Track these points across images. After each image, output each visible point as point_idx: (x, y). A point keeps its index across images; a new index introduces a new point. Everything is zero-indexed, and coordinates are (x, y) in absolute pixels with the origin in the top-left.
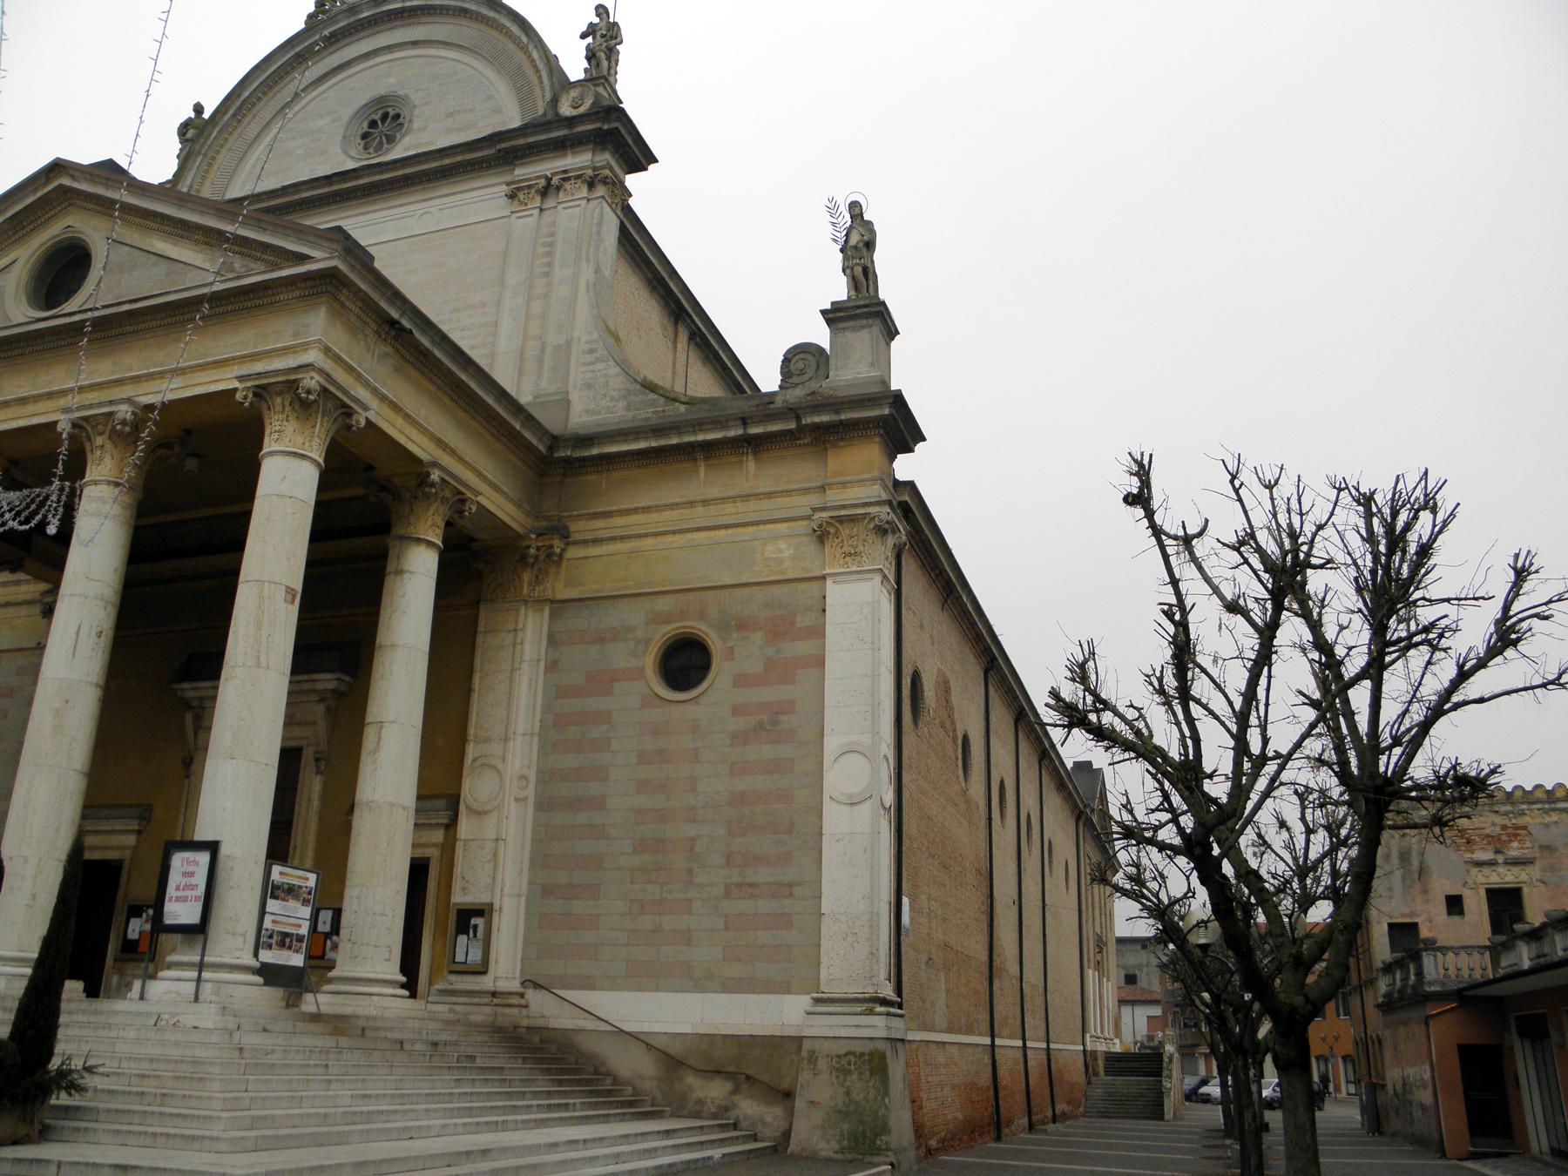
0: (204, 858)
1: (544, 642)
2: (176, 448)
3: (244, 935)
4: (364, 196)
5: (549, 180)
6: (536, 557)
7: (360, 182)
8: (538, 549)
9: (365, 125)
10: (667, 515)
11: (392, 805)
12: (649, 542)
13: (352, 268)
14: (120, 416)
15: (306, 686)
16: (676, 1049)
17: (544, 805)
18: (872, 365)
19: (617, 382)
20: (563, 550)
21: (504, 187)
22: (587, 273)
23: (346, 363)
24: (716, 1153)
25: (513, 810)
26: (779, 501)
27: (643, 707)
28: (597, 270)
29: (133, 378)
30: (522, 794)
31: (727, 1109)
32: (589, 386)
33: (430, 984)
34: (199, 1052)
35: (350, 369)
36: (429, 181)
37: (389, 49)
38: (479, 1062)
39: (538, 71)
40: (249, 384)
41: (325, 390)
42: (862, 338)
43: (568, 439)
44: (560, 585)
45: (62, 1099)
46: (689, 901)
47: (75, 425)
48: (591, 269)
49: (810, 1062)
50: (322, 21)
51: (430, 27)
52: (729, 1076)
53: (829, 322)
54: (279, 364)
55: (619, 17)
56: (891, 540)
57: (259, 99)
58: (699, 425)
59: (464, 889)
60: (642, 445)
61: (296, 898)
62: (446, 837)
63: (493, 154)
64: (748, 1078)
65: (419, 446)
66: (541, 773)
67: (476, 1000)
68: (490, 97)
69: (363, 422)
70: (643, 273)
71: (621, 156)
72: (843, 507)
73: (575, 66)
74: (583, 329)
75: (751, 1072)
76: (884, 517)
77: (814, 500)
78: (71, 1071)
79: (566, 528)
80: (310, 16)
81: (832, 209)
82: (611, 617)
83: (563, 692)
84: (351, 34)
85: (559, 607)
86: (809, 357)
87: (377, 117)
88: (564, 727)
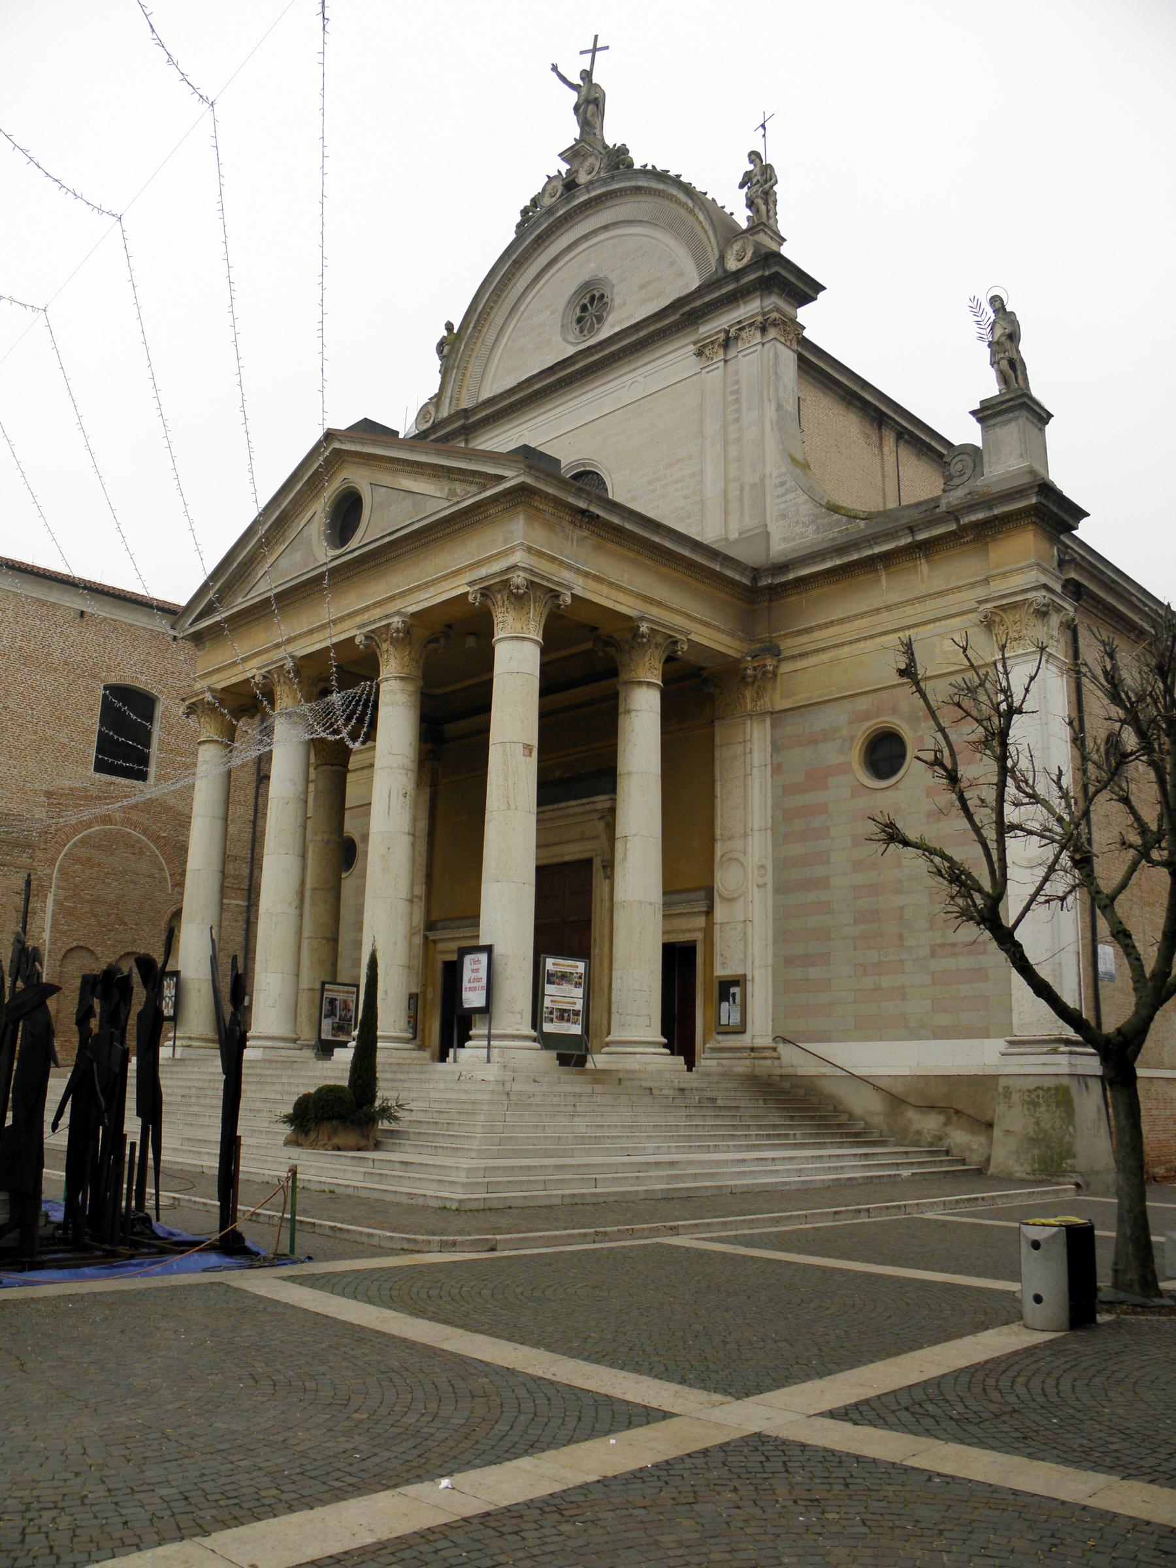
0: (483, 957)
1: (769, 749)
2: (442, 641)
3: (521, 1013)
4: (582, 377)
5: (727, 332)
6: (755, 677)
7: (577, 366)
8: (755, 669)
9: (578, 310)
10: (858, 623)
11: (640, 902)
12: (846, 650)
13: (537, 478)
14: (394, 626)
15: (588, 807)
16: (898, 1089)
17: (781, 888)
18: (1021, 456)
19: (807, 509)
20: (776, 667)
21: (692, 347)
22: (770, 412)
23: (548, 555)
24: (905, 1173)
25: (756, 895)
26: (951, 598)
27: (853, 796)
28: (779, 408)
29: (400, 593)
30: (761, 881)
31: (940, 1139)
32: (783, 516)
33: (704, 1044)
34: (479, 1096)
35: (553, 559)
36: (632, 353)
37: (585, 237)
38: (720, 1103)
39: (706, 232)
40: (476, 588)
41: (532, 582)
42: (1012, 431)
43: (766, 570)
44: (777, 698)
45: (384, 1125)
46: (902, 961)
47: (367, 637)
48: (773, 409)
49: (1005, 1096)
50: (528, 228)
51: (616, 209)
52: (942, 1110)
53: (979, 420)
54: (496, 567)
55: (769, 160)
56: (1055, 620)
57: (492, 308)
58: (873, 539)
59: (723, 964)
60: (828, 565)
61: (569, 982)
62: (707, 921)
63: (679, 318)
64: (957, 1112)
65: (626, 606)
66: (775, 860)
67: (738, 1055)
68: (672, 263)
69: (569, 600)
70: (835, 392)
71: (788, 295)
72: (1004, 596)
73: (742, 217)
74: (774, 466)
75: (959, 1107)
76: (1041, 600)
77: (980, 592)
78: (390, 1108)
79: (778, 647)
80: (519, 226)
81: (976, 308)
82: (821, 721)
83: (788, 790)
84: (553, 233)
85: (777, 717)
86: (965, 457)
87: (586, 301)
88: (793, 821)
